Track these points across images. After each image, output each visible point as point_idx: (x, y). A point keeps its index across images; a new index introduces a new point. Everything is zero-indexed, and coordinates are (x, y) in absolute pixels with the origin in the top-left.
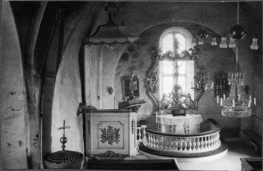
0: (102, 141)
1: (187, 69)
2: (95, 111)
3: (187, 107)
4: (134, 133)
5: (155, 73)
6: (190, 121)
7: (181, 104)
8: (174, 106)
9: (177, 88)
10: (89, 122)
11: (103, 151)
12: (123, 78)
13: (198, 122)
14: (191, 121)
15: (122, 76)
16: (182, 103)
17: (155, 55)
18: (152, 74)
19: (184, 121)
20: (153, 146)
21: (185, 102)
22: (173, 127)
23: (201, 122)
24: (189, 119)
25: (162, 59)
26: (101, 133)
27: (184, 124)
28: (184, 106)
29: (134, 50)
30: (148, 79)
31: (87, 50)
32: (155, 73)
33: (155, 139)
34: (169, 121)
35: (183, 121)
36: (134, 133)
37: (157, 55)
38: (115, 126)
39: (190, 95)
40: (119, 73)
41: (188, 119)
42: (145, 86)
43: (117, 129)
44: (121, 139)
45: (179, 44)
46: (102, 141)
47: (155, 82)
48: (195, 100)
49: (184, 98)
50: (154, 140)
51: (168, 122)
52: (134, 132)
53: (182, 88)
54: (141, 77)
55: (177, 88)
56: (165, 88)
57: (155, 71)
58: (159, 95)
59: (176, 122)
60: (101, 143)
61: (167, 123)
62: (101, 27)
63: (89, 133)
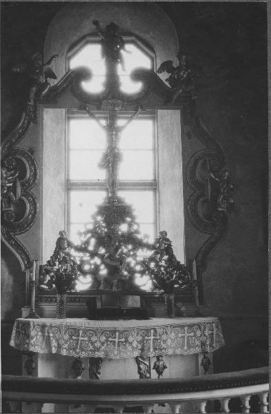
3: (157, 291)
5: (23, 153)
6: (165, 341)
8: (101, 287)
9: (115, 212)
13: (203, 344)
14: (169, 342)
16: (138, 275)
19: (140, 338)
21: (146, 269)
22: (86, 365)
23: (216, 346)
24: (159, 331)
25: (53, 99)
27: (136, 353)
28: (145, 283)
34: (66, 337)
35: (130, 339)
39: (168, 240)
41: (155, 329)
45: (122, 62)
47: (23, 185)
48: (189, 260)
49: (144, 254)
51: (62, 342)
53: (135, 213)
55: (115, 212)
58: (38, 242)
59: (98, 345)
61: (59, 347)
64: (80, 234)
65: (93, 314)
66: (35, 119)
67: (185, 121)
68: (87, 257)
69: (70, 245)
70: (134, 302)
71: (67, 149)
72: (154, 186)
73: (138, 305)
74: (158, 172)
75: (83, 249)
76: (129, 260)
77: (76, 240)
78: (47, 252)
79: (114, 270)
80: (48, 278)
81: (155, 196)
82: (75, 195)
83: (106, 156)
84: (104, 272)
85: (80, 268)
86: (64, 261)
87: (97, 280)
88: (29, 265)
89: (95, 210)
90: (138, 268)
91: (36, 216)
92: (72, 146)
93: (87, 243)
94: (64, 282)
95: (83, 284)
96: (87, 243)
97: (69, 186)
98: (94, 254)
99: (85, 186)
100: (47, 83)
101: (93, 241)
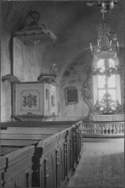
0: (24, 105)
1: (115, 81)
2: (20, 83)
4: (48, 100)
5: (89, 85)
7: (111, 108)
9: (107, 95)
10: (15, 91)
11: (25, 113)
12: (66, 89)
15: (65, 87)
17: (90, 72)
18: (88, 85)
20: (83, 133)
21: (114, 106)
25: (94, 74)
26: (23, 99)
29: (77, 73)
30: (84, 89)
31: (15, 39)
32: (89, 85)
33: (87, 127)
36: (48, 100)
37: (91, 71)
38: (34, 94)
40: (63, 85)
42: (83, 94)
43: (35, 96)
44: (38, 103)
46: (24, 105)
47: (90, 91)
48: (122, 104)
50: (84, 128)
52: (48, 98)
54: (79, 87)
55: (107, 95)
56: (98, 95)
57: (90, 83)
60: (23, 107)
61: (98, 120)
62: (26, 26)
63: (15, 100)
64: (101, 99)
65: (104, 114)
66: (91, 78)
67: (120, 76)
68: (102, 104)
69: (99, 101)
70: (111, 112)
71: (98, 81)
72: (116, 88)
73: (112, 112)
74: (67, 163)
75: (101, 102)
76: (110, 104)
77: (100, 101)
78: (95, 103)
79: (108, 106)
80: (95, 108)
81: (116, 91)
82: (100, 91)
83: (105, 85)
84: (106, 106)
85: (101, 106)
86: (98, 105)
87: (104, 108)
88: (92, 105)
89: (103, 95)
90: (112, 106)
91: (92, 97)
92: (99, 81)
93: (102, 101)
94: (98, 109)
95: (102, 109)
96: (102, 101)
97: (98, 89)
98: (103, 103)
99: (101, 89)
100: (93, 71)
101: (103, 101)
